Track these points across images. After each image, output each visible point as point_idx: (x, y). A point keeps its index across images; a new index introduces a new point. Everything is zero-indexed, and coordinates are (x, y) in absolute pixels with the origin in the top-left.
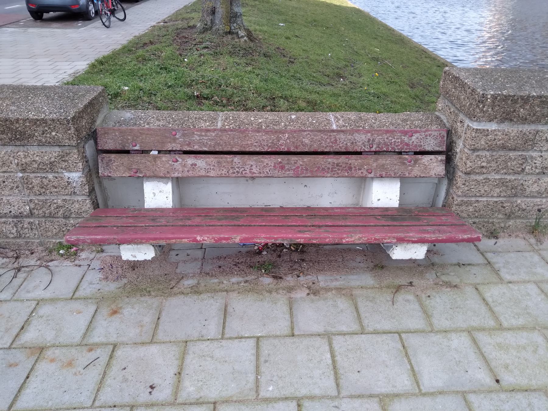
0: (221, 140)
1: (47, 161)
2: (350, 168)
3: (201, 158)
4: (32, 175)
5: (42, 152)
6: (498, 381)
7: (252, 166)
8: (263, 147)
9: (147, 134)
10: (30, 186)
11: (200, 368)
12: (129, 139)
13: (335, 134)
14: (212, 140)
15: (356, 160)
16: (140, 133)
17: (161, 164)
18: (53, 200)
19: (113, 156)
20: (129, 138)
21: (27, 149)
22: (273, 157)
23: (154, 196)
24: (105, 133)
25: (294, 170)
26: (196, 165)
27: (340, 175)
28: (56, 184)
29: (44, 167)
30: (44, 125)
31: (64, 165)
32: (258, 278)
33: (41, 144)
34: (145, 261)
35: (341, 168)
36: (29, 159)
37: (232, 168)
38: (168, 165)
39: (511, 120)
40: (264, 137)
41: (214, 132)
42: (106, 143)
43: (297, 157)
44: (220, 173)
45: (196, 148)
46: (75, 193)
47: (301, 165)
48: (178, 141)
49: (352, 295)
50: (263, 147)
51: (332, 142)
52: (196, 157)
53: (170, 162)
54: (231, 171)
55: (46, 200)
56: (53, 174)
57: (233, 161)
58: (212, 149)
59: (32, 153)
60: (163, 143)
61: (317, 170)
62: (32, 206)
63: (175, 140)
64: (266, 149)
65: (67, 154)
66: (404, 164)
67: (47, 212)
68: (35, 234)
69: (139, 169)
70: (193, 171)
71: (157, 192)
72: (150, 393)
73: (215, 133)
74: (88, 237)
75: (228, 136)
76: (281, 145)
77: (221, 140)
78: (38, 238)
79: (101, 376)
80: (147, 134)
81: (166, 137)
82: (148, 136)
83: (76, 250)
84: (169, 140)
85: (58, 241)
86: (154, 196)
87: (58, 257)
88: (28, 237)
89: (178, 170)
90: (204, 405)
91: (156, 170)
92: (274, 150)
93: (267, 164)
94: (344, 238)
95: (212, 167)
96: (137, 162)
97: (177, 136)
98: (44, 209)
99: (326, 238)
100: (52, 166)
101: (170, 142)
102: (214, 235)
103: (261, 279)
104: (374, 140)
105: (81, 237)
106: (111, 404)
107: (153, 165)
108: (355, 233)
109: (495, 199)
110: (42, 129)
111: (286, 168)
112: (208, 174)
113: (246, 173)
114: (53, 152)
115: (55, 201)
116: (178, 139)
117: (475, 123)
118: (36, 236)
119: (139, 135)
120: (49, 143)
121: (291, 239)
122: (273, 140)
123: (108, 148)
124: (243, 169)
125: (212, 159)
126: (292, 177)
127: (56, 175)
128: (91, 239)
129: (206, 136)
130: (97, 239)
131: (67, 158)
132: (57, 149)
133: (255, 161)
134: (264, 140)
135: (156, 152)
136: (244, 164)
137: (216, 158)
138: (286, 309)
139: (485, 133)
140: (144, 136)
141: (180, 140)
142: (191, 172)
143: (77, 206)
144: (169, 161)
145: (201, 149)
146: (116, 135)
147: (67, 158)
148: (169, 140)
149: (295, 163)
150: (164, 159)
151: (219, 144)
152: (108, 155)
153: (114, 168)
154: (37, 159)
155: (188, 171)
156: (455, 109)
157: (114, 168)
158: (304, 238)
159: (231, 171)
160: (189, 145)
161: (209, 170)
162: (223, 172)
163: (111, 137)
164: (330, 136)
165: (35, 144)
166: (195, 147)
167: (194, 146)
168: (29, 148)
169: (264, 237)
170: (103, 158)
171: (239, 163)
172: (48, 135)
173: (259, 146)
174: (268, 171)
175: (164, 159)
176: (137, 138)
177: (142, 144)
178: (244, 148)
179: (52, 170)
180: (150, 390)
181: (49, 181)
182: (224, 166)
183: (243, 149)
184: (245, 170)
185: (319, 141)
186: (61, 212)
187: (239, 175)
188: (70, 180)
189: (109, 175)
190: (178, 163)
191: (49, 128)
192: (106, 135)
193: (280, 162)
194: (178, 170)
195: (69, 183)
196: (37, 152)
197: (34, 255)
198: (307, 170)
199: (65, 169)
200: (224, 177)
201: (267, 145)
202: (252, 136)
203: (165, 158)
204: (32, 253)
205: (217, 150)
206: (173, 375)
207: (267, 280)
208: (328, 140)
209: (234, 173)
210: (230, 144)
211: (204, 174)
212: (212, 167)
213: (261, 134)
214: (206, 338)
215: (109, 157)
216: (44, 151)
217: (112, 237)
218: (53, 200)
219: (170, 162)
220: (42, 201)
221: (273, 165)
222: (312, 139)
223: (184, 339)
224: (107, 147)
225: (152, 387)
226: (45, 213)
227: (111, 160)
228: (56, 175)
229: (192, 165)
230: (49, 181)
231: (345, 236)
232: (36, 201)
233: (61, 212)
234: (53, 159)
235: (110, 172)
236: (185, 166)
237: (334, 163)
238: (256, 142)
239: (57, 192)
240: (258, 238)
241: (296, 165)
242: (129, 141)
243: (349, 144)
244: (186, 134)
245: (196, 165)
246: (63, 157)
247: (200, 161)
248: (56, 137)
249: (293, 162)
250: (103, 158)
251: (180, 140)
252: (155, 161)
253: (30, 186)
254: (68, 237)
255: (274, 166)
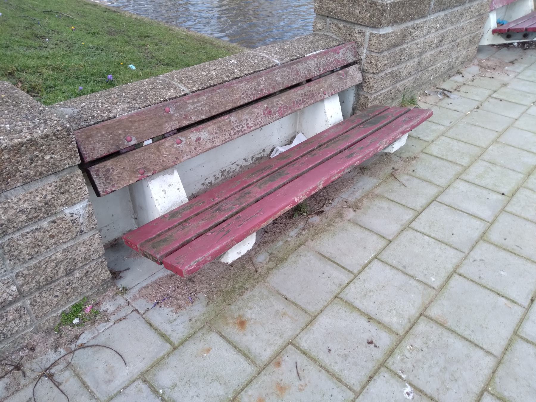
0: (213, 101)
1: (40, 202)
2: (313, 95)
3: (203, 129)
4: (17, 235)
5: (31, 193)
6: (503, 194)
7: (247, 120)
8: (250, 97)
9: (139, 121)
10: (16, 253)
11: (376, 303)
12: (120, 134)
13: (295, 66)
14: (206, 104)
15: (314, 86)
16: (131, 122)
17: (166, 152)
18: (50, 257)
19: (109, 163)
20: (120, 132)
21: (6, 197)
22: (260, 103)
23: (165, 193)
24: (88, 137)
25: (278, 111)
26: (200, 139)
27: (309, 103)
28: (54, 231)
29: (35, 215)
30: (33, 148)
31: (63, 198)
32: (307, 221)
33: (28, 180)
34: (249, 252)
35: (307, 97)
36: (11, 212)
37: (232, 129)
38: (174, 150)
39: (397, 22)
40: (248, 86)
41: (204, 95)
42: (94, 149)
43: (277, 98)
44: (223, 139)
45: (194, 119)
46: (81, 231)
47: (282, 105)
48: (174, 118)
49: (377, 195)
50: (250, 97)
51: (295, 75)
52: (197, 130)
53: (175, 146)
54: (232, 133)
55: (40, 263)
56: (49, 219)
57: (230, 121)
58: (209, 115)
59: (15, 200)
60: (160, 125)
61: (293, 105)
62: (20, 281)
63: (170, 117)
64: (253, 98)
65: (67, 181)
66: (341, 78)
67: (42, 279)
68: (26, 322)
69: (145, 168)
70: (199, 146)
71: (165, 187)
72: (376, 346)
73: (206, 96)
74: (207, 255)
75: (218, 95)
76: (262, 90)
77: (213, 101)
78: (31, 325)
79: (323, 371)
80: (139, 121)
81: (160, 116)
82: (141, 122)
83: (92, 308)
84: (164, 120)
85: (60, 312)
86: (165, 193)
87: (78, 330)
88: (17, 331)
89: (185, 152)
90: (419, 321)
91: (163, 161)
92: (258, 97)
93: (258, 113)
94: (378, 147)
95: (215, 136)
96: (140, 160)
97: (171, 112)
98: (38, 277)
99: (369, 153)
100: (48, 207)
101: (166, 122)
102: (305, 191)
103: (309, 220)
104: (320, 63)
105: (201, 258)
106: (366, 379)
107: (159, 156)
108: (382, 138)
109: (388, 89)
110: (28, 155)
111: (273, 111)
112: (214, 145)
113: (245, 130)
114: (47, 186)
115: (53, 257)
116: (173, 115)
117: (381, 30)
118: (28, 323)
119: (130, 124)
120: (41, 174)
121: (351, 165)
122: (255, 87)
123: (99, 156)
124: (241, 127)
125: (212, 126)
126: (279, 119)
127: (53, 218)
128: (211, 255)
129: (198, 102)
130: (217, 251)
131: (67, 187)
132: (53, 179)
133: (248, 113)
134: (248, 89)
135: (150, 141)
136: (241, 120)
137: (215, 123)
138: (358, 229)
139: (385, 36)
140: (136, 124)
141: (176, 115)
142: (198, 149)
143: (83, 249)
144: (173, 144)
145: (199, 119)
146: (103, 135)
147: (67, 187)
148: (164, 120)
149: (277, 104)
150: (167, 144)
151: (213, 107)
152: (102, 165)
153: (116, 177)
154: (26, 205)
155: (195, 149)
156: (345, 24)
157: (116, 177)
158: (359, 160)
159: (232, 133)
160: (186, 118)
161: (214, 140)
162: (226, 137)
163: (96, 139)
164: (293, 68)
165: (19, 184)
166: (193, 119)
167: (191, 118)
168: (9, 195)
169: (337, 173)
170: (98, 171)
171: (236, 121)
172: (40, 162)
173: (246, 97)
174: (260, 120)
175: (167, 144)
176: (129, 129)
177: (138, 136)
178: (235, 103)
179: (49, 214)
180: (372, 346)
181: (44, 232)
182: (225, 130)
183: (235, 105)
184: (243, 127)
185: (287, 76)
186: (62, 269)
187: (240, 134)
188: (75, 217)
189: (114, 189)
190: (183, 143)
191: (41, 151)
192: (90, 139)
193: (267, 108)
194: (185, 152)
195: (73, 221)
196: (24, 196)
197: (38, 349)
198: (287, 108)
199: (66, 204)
200: (228, 141)
201: (252, 93)
202: (238, 88)
203: (168, 142)
204: (33, 349)
205: (214, 114)
206: (368, 324)
207: (315, 219)
208: (293, 73)
209: (235, 134)
210: (222, 104)
211: (210, 146)
212: (215, 136)
213: (244, 84)
214: (345, 285)
215: (105, 167)
216: (33, 190)
217: (229, 240)
218: (50, 257)
219: (175, 146)
220: (35, 266)
221: (262, 113)
222: (282, 75)
223: (332, 297)
224: (97, 155)
225: (370, 343)
226: (39, 283)
227: (108, 170)
228: (53, 218)
229: (196, 141)
230: (44, 232)
231: (378, 145)
232: (25, 272)
233: (62, 269)
234: (49, 197)
235: (113, 186)
236: (190, 144)
237: (302, 94)
238: (243, 94)
239: (55, 243)
240: (333, 176)
241: (279, 106)
242: (122, 137)
243: (306, 72)
244: (179, 106)
245: (200, 139)
246: (61, 190)
247: (202, 133)
248: (52, 160)
249: (275, 104)
250: (98, 171)
251: (176, 115)
252: (159, 151)
253: (16, 253)
254: (186, 267)
255: (264, 114)
